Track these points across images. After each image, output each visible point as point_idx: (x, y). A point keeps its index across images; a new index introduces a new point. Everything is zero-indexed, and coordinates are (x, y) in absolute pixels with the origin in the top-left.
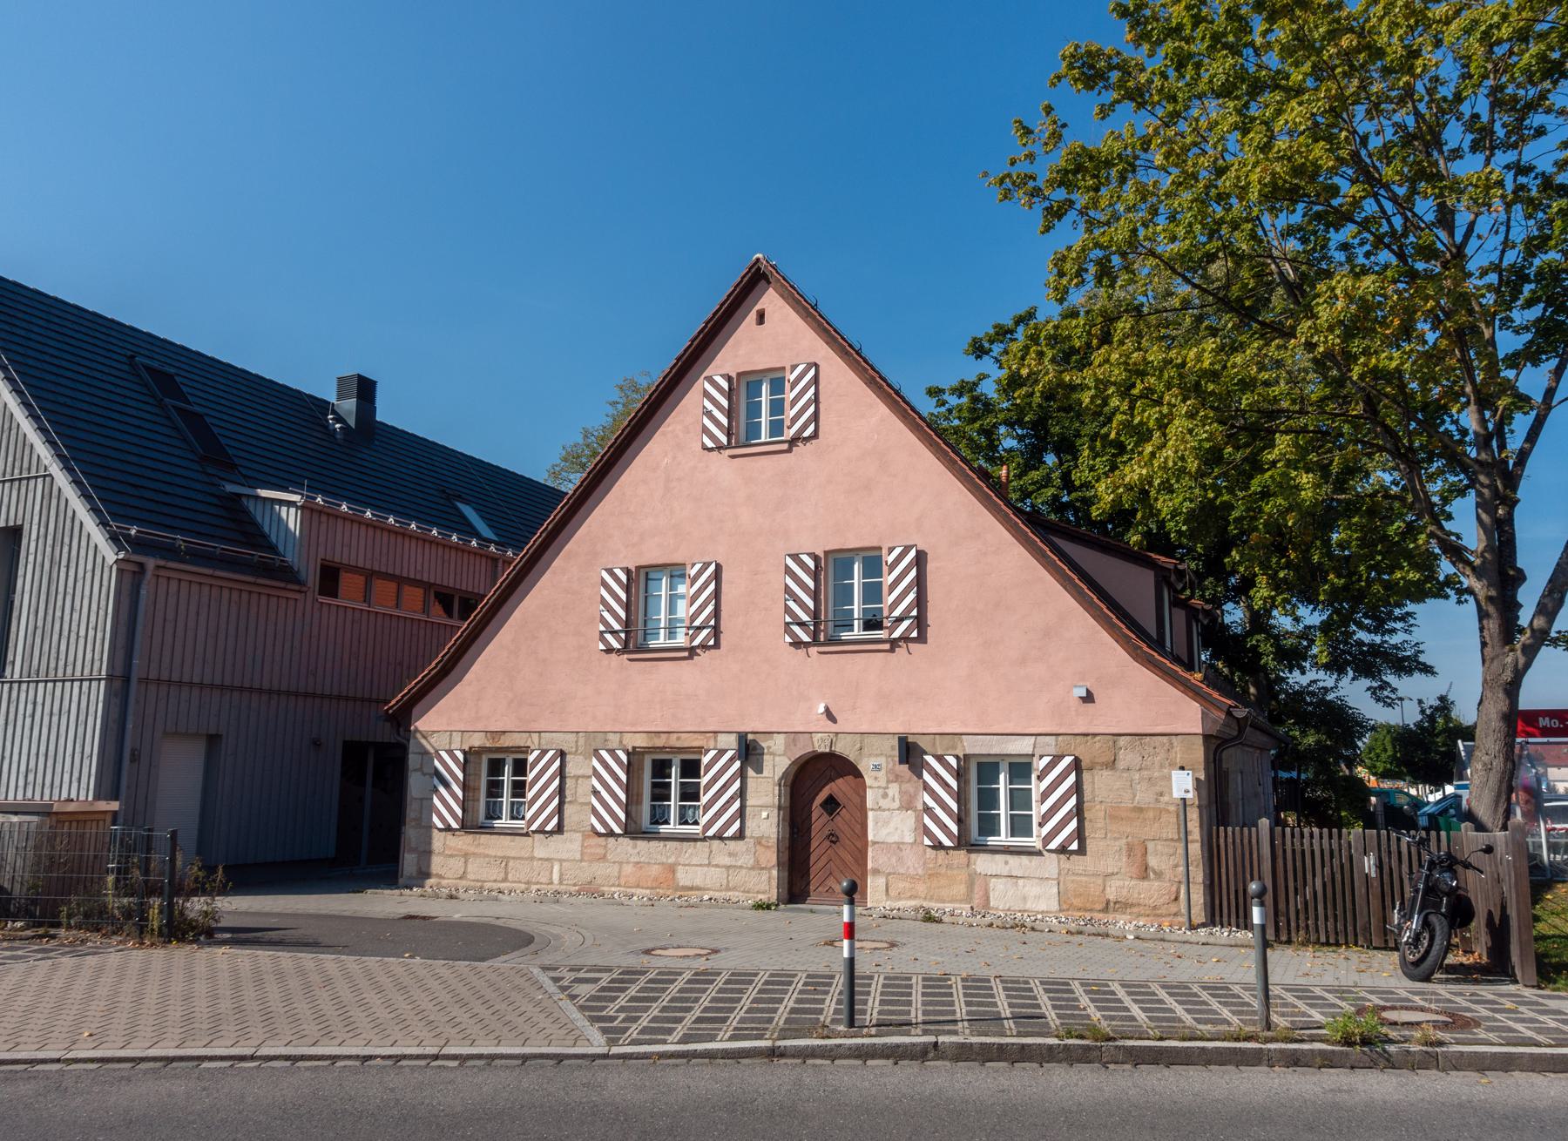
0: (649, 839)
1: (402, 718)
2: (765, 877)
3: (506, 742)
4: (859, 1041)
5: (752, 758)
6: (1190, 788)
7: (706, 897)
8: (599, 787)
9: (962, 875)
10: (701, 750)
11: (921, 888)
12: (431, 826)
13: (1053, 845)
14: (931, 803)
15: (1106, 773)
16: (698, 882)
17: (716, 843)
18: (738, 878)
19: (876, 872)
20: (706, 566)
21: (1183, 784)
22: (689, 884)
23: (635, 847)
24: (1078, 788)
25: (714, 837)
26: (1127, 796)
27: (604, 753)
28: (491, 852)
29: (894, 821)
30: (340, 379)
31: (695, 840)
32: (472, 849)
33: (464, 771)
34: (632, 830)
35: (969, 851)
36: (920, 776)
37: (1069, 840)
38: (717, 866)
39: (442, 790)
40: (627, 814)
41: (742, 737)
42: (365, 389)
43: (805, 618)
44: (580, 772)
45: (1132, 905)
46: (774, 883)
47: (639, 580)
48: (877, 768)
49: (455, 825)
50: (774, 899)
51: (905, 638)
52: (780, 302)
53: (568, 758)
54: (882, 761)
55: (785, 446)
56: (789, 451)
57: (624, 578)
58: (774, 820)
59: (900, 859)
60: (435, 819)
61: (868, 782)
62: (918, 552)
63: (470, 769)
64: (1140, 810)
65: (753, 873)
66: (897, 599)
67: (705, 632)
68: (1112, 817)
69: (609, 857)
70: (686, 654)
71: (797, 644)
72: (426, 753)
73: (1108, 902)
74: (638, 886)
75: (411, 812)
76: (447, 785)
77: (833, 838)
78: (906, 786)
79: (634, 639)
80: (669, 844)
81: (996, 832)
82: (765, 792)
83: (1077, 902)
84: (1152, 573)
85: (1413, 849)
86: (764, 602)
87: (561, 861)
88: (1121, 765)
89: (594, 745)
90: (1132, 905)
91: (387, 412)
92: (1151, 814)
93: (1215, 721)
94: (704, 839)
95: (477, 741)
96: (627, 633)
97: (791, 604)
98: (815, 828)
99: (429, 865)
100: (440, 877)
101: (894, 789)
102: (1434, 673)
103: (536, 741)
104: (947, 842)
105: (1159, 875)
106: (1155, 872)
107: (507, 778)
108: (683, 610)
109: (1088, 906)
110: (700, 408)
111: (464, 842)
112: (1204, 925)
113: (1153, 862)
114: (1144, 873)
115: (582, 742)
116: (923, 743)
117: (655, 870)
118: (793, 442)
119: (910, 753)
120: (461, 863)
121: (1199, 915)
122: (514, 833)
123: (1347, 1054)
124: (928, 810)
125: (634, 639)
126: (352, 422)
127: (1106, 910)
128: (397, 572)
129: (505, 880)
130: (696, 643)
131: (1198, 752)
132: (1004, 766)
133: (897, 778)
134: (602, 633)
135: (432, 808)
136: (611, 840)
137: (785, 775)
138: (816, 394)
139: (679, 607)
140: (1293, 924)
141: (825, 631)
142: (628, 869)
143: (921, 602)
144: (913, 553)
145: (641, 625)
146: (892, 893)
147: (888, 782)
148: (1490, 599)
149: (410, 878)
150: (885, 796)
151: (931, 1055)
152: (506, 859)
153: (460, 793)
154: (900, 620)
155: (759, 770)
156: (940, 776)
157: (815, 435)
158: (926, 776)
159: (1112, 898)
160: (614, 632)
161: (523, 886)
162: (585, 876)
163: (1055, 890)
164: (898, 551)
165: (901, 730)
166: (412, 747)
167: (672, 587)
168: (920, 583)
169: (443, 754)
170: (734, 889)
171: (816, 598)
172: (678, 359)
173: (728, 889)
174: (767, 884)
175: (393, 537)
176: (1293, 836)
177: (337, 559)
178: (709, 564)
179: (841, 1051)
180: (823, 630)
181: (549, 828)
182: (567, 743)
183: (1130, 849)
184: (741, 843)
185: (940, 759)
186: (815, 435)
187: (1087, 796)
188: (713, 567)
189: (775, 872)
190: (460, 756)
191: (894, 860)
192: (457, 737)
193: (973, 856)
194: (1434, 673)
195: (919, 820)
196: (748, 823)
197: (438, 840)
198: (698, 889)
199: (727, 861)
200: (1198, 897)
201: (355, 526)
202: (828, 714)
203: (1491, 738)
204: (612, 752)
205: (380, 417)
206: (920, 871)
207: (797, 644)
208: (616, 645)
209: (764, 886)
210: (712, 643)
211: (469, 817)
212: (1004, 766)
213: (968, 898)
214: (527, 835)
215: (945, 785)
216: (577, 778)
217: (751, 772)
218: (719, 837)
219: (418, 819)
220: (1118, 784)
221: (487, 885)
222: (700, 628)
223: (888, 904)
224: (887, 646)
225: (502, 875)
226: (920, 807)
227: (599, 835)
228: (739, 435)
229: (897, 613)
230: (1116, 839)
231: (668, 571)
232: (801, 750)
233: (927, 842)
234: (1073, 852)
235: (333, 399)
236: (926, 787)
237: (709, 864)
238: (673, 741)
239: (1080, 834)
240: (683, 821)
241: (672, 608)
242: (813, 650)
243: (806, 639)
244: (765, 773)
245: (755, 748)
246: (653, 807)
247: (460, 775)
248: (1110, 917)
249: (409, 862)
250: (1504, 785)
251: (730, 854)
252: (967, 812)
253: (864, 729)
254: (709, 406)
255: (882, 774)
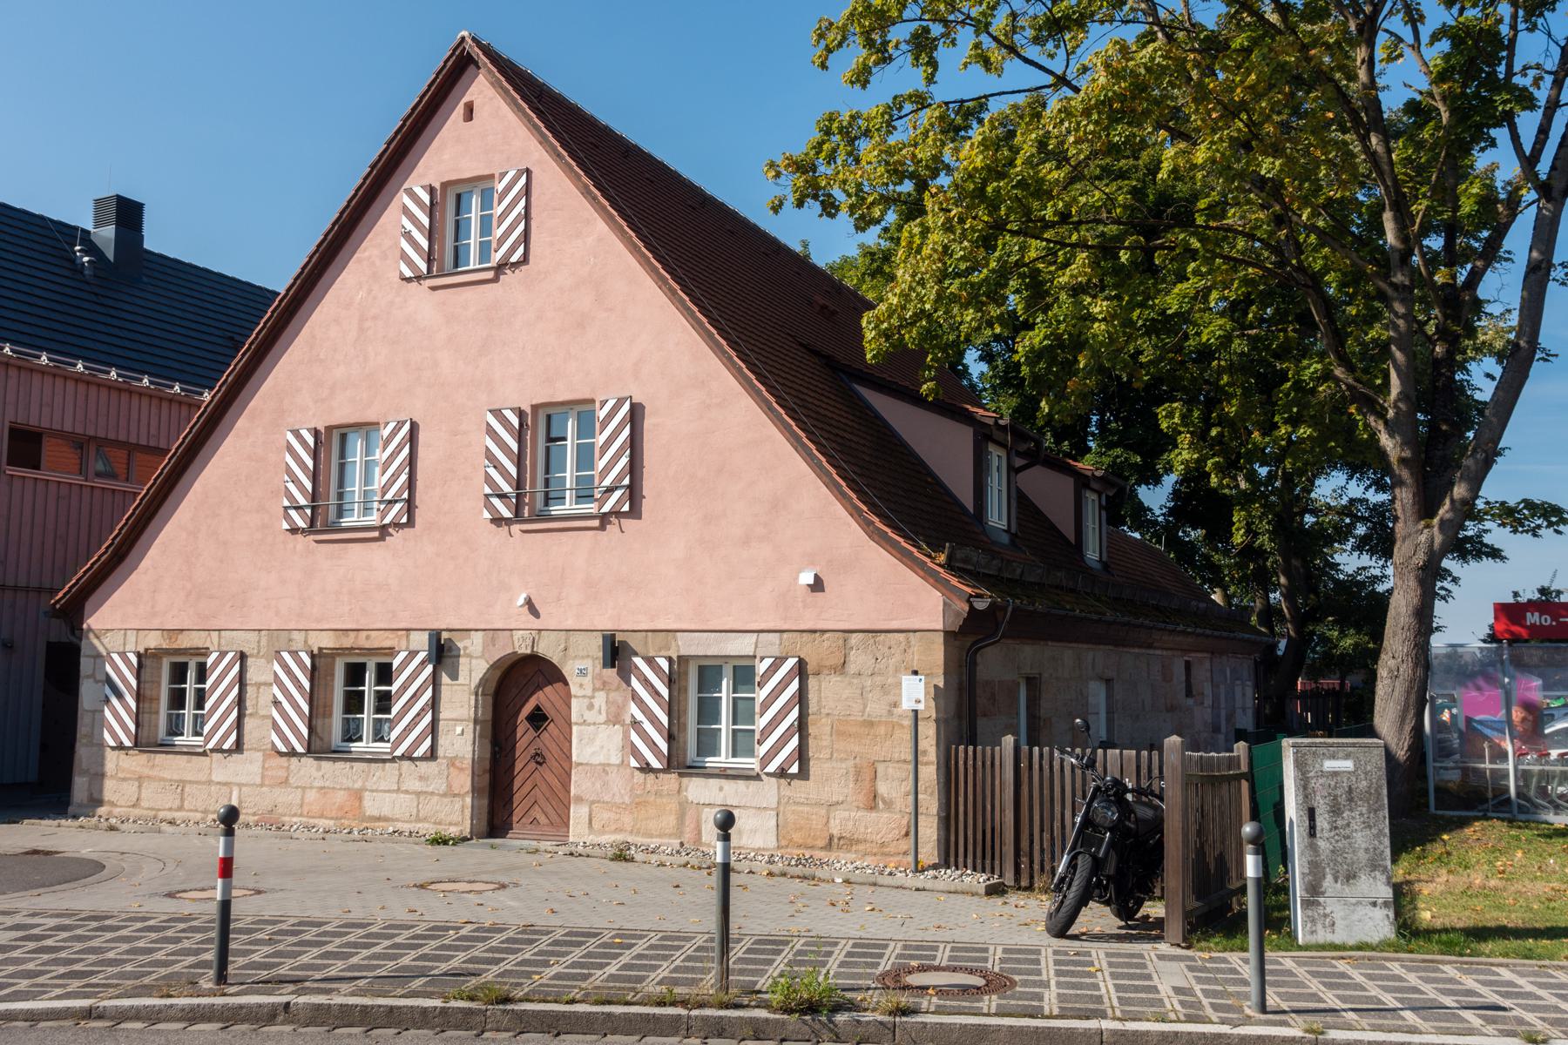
0: (335, 760)
1: (74, 612)
2: (458, 806)
3: (185, 642)
4: (196, 1001)
5: (447, 661)
6: (922, 697)
7: (391, 830)
8: (281, 697)
9: (673, 805)
10: (392, 652)
11: (627, 820)
12: (102, 745)
13: (771, 768)
14: (640, 716)
15: (835, 679)
16: (386, 812)
17: (406, 764)
18: (432, 806)
19: (580, 799)
20: (400, 424)
21: (915, 693)
22: (376, 813)
23: (319, 769)
24: (802, 697)
25: (402, 757)
26: (857, 707)
27: (286, 655)
28: (166, 775)
29: (602, 734)
30: (97, 201)
31: (384, 761)
32: (146, 771)
33: (138, 678)
34: (317, 748)
35: (681, 775)
36: (628, 683)
37: (789, 761)
38: (407, 792)
39: (114, 701)
40: (311, 728)
41: (435, 635)
42: (128, 214)
43: (507, 488)
44: (262, 679)
45: (858, 842)
46: (468, 813)
47: (331, 445)
48: (582, 673)
49: (127, 743)
50: (467, 833)
51: (616, 513)
52: (491, 92)
53: (250, 661)
54: (586, 664)
55: (490, 275)
56: (495, 280)
57: (311, 441)
58: (469, 736)
59: (605, 784)
60: (107, 735)
61: (574, 689)
62: (632, 405)
63: (146, 675)
64: (870, 724)
65: (446, 800)
66: (610, 467)
67: (398, 506)
68: (841, 734)
69: (292, 781)
70: (376, 534)
71: (498, 521)
72: (99, 656)
73: (831, 838)
74: (322, 816)
75: (83, 729)
76: (120, 696)
77: (539, 759)
78: (613, 695)
79: (322, 517)
80: (357, 765)
81: (714, 751)
82: (461, 703)
83: (797, 837)
84: (970, 430)
85: (1078, 772)
86: (467, 468)
87: (240, 785)
88: (852, 668)
89: (278, 642)
90: (858, 842)
91: (157, 238)
92: (882, 730)
93: (958, 614)
94: (393, 760)
95: (153, 641)
96: (313, 508)
97: (492, 471)
98: (520, 746)
99: (101, 791)
100: (113, 804)
101: (600, 699)
102: (1503, 558)
103: (216, 641)
104: (656, 764)
105: (889, 804)
106: (884, 802)
107: (369, 688)
108: (379, 480)
109: (810, 842)
110: (400, 223)
111: (136, 762)
112: (935, 867)
113: (882, 788)
114: (873, 801)
115: (264, 642)
116: (634, 642)
117: (340, 797)
118: (500, 268)
119: (616, 653)
120: (135, 788)
121: (929, 851)
122: (191, 753)
123: (784, 1023)
124: (635, 724)
125: (322, 517)
126: (110, 255)
127: (829, 846)
128: (122, 437)
129: (181, 808)
130: (387, 520)
131: (935, 654)
132: (728, 672)
133: (605, 686)
134: (286, 508)
135: (103, 722)
136: (294, 760)
137: (483, 682)
138: (527, 208)
139: (373, 475)
140: (1036, 867)
141: (532, 505)
142: (311, 795)
143: (635, 468)
144: (626, 407)
145: (333, 500)
146: (596, 826)
147: (595, 690)
148: (1402, 461)
149: (80, 805)
150: (590, 707)
151: (281, 1018)
152: (182, 783)
153: (133, 704)
154: (610, 490)
155: (454, 676)
156: (650, 678)
157: (525, 259)
158: (635, 683)
159: (836, 832)
160: (298, 508)
161: (199, 816)
162: (266, 804)
163: (774, 822)
164: (611, 403)
165: (609, 626)
166: (84, 650)
167: (368, 451)
168: (635, 444)
169: (115, 657)
170: (425, 820)
171: (519, 464)
172: (373, 167)
173: (418, 820)
174: (458, 814)
175: (114, 395)
176: (1041, 756)
177: (33, 421)
178: (404, 423)
179: (172, 1012)
180: (528, 503)
181: (226, 746)
182: (248, 642)
183: (858, 773)
184: (432, 764)
185: (650, 661)
186: (525, 259)
187: (813, 708)
188: (407, 427)
189: (468, 800)
190: (134, 660)
191: (598, 785)
192: (131, 636)
193: (685, 780)
194: (1503, 558)
195: (626, 736)
196: (441, 741)
197: (112, 761)
198: (386, 819)
199: (417, 786)
200: (930, 831)
201: (59, 382)
202: (530, 604)
203: (1401, 636)
204: (294, 654)
205: (149, 244)
206: (627, 799)
207: (498, 521)
208: (301, 524)
209: (456, 817)
210: (404, 520)
211: (144, 733)
212: (728, 672)
213: (679, 832)
214: (204, 754)
215: (655, 693)
216: (258, 685)
217: (445, 679)
218: (218, 750)
219: (91, 735)
220: (847, 693)
221: (162, 815)
222: (392, 502)
223: (590, 839)
224: (596, 523)
225: (177, 803)
226: (628, 721)
227: (281, 754)
228: (443, 259)
229: (607, 482)
230: (842, 760)
231: (363, 432)
232: (500, 651)
233: (634, 763)
234: (793, 776)
235: (89, 226)
236: (635, 697)
237: (398, 790)
238: (363, 641)
239: (802, 754)
240: (379, 737)
241: (368, 479)
242: (516, 528)
243: (507, 514)
244: (461, 680)
245: (450, 649)
246: (170, 716)
247: (134, 683)
248: (832, 856)
249: (80, 785)
250: (1413, 697)
251: (421, 778)
252: (683, 727)
253: (569, 624)
254: (409, 226)
255: (587, 681)
